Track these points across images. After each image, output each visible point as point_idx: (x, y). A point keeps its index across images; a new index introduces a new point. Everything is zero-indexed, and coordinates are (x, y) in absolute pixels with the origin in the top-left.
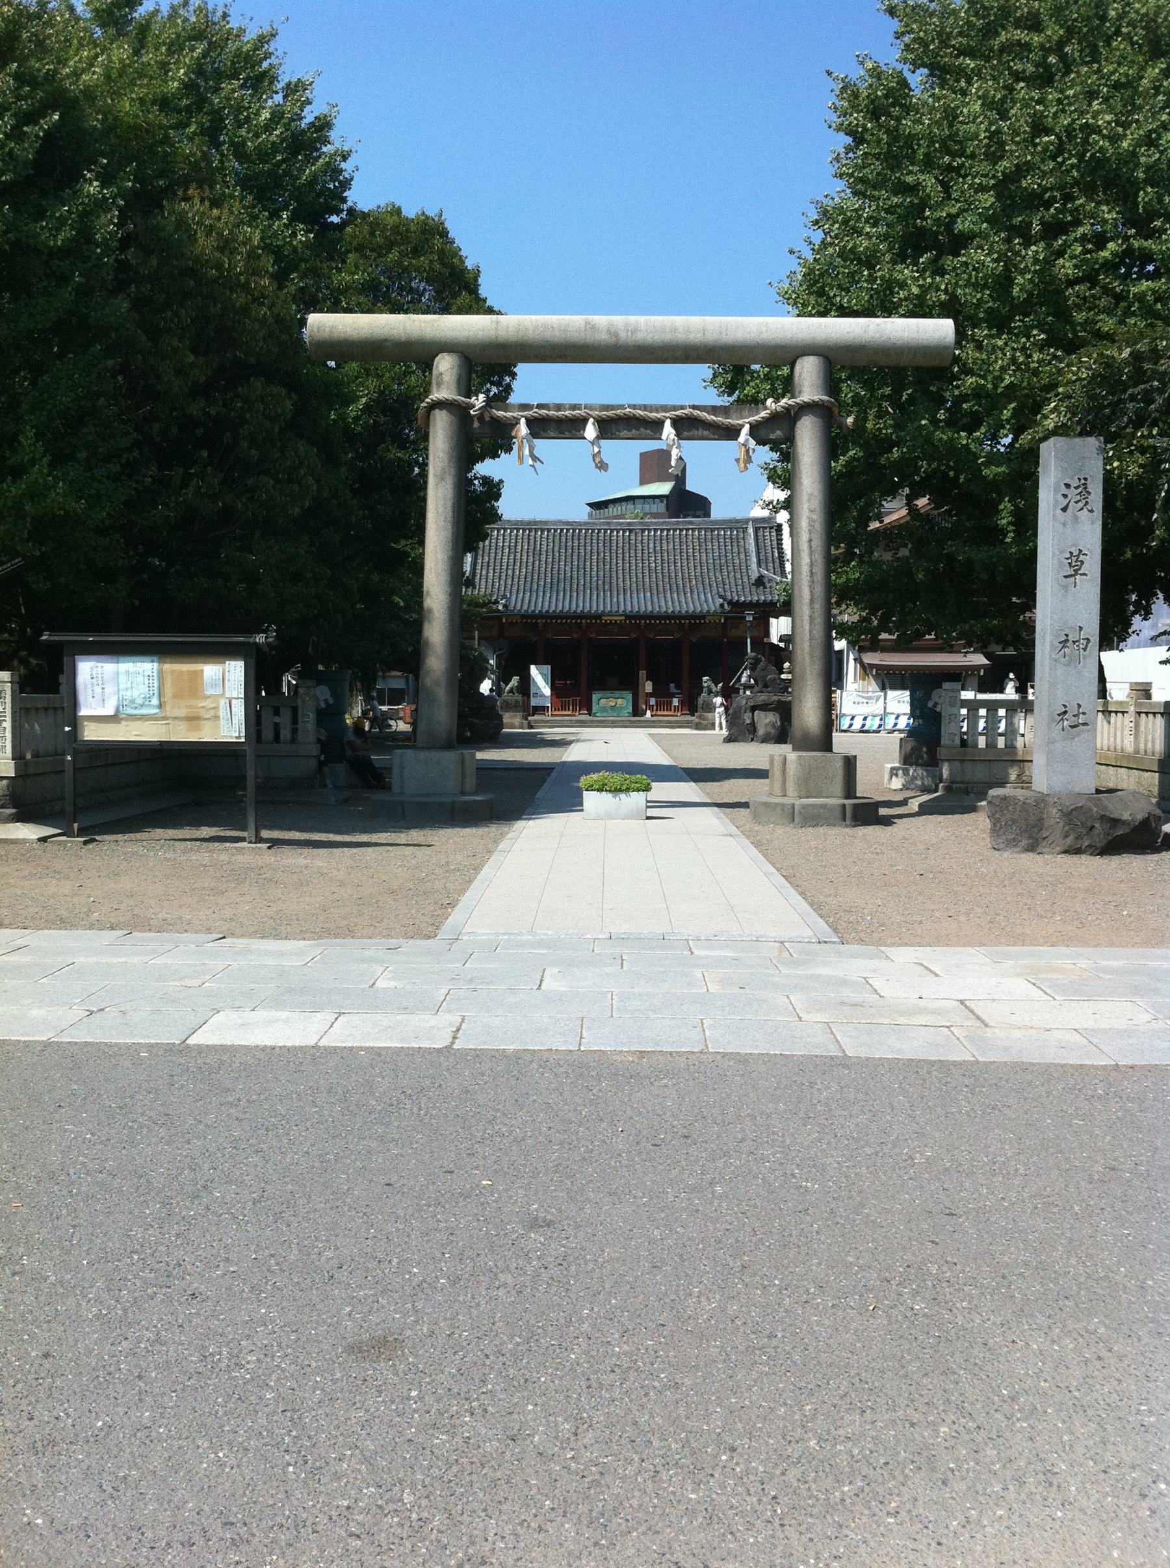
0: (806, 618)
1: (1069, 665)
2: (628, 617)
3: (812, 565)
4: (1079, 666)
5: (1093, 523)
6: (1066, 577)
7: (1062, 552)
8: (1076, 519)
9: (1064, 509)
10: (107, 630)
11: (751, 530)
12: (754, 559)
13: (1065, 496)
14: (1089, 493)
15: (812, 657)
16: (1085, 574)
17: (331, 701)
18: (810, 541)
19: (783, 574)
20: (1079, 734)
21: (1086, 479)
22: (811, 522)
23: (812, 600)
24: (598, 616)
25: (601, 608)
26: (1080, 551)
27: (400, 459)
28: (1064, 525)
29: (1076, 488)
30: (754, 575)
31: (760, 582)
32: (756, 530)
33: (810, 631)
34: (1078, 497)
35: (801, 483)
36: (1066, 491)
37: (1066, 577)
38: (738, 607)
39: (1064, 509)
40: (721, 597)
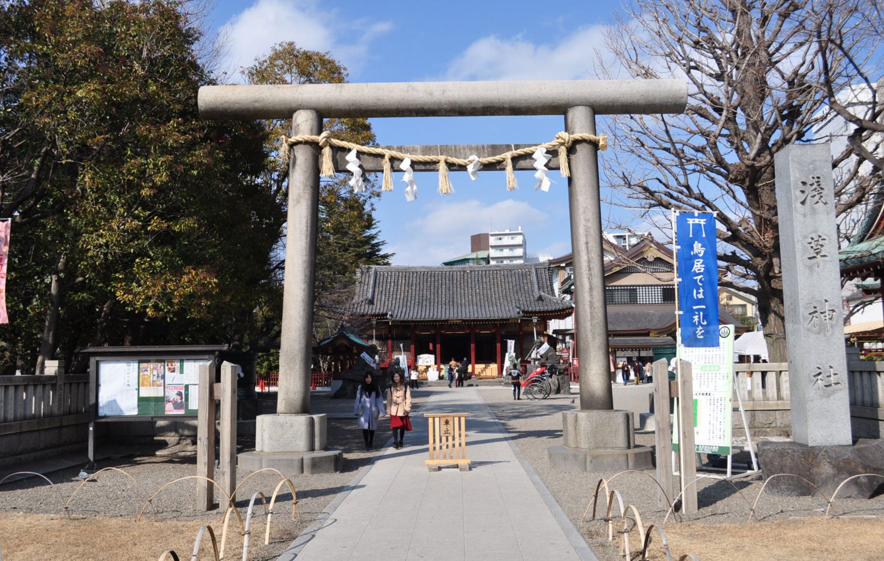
0: (587, 303)
1: (819, 333)
2: (463, 320)
3: (589, 261)
4: (828, 334)
5: (828, 214)
6: (810, 258)
7: (815, 232)
8: (814, 211)
9: (803, 203)
10: (168, 343)
11: (533, 270)
12: (536, 286)
13: (803, 192)
14: (822, 189)
15: (594, 334)
16: (825, 256)
17: (242, 375)
18: (587, 243)
19: (553, 294)
20: (833, 392)
21: (818, 178)
22: (587, 230)
23: (591, 289)
24: (447, 321)
25: (456, 316)
26: (820, 236)
27: (223, 182)
28: (805, 216)
29: (812, 185)
30: (537, 295)
31: (540, 298)
32: (536, 270)
33: (591, 313)
34: (815, 193)
35: (577, 200)
36: (803, 188)
37: (810, 258)
38: (528, 314)
39: (803, 203)
40: (519, 308)
